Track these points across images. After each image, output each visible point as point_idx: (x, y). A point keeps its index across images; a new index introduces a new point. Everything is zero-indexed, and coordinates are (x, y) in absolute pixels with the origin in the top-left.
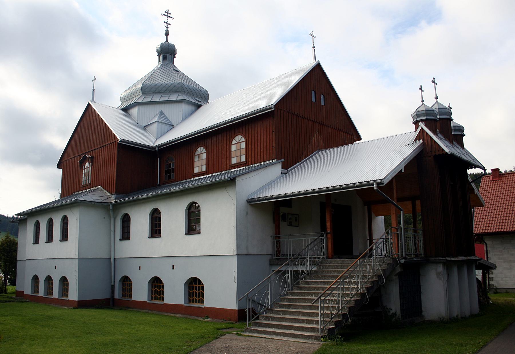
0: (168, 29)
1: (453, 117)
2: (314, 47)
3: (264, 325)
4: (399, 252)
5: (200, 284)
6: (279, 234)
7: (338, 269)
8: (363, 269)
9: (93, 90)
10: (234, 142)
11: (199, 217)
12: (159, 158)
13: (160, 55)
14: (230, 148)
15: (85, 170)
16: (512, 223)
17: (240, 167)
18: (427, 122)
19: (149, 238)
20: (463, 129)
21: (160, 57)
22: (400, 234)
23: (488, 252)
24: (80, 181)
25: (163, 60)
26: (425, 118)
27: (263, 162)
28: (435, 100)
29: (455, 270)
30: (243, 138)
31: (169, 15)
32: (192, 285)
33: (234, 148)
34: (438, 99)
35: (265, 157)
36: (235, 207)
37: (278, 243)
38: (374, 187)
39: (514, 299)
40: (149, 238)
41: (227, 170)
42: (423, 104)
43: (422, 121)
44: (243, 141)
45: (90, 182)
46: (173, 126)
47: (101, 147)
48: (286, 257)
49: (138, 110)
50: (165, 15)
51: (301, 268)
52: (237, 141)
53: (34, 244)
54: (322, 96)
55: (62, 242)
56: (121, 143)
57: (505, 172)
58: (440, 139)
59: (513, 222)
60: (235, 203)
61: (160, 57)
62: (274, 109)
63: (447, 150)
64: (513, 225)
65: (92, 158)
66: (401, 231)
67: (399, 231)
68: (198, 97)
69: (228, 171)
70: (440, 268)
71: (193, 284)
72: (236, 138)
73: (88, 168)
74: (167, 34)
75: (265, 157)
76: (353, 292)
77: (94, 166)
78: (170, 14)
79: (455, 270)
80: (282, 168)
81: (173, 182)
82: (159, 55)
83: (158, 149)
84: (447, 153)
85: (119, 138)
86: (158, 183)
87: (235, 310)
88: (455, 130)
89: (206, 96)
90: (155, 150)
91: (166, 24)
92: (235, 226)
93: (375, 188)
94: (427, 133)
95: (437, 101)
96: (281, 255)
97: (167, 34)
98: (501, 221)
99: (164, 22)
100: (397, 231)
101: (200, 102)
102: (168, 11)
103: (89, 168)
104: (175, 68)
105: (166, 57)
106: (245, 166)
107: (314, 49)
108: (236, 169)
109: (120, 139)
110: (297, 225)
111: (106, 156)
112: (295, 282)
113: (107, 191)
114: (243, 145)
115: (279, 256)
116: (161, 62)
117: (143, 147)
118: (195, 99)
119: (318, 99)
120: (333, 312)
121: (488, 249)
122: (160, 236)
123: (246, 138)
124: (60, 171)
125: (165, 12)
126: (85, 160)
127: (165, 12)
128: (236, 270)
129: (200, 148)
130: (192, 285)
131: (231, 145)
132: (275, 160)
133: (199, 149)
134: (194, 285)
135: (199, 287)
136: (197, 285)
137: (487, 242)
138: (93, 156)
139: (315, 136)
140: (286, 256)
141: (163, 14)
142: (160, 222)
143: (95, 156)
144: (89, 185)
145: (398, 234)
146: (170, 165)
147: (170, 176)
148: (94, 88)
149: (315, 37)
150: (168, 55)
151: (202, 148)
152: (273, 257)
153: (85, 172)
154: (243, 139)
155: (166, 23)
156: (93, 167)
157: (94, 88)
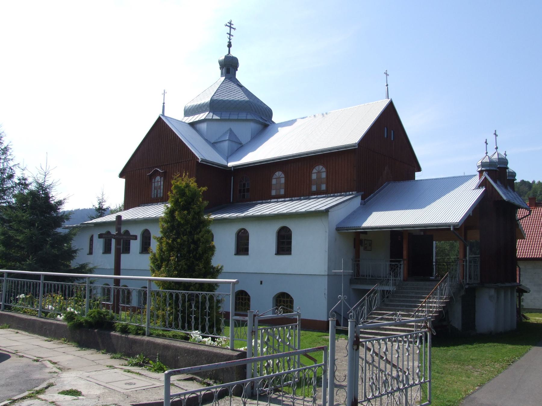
0: (231, 41)
1: (509, 166)
2: (387, 85)
3: (365, 333)
4: (463, 279)
5: (288, 298)
6: (359, 258)
7: (415, 290)
8: (113, 241)
9: (164, 103)
10: (315, 171)
12: (232, 177)
13: (223, 68)
14: (310, 176)
15: (156, 183)
18: (490, 172)
19: (235, 255)
20: (515, 175)
21: (224, 69)
22: (466, 264)
23: (521, 276)
24: (270, 192)
25: (226, 73)
26: (488, 168)
27: (343, 192)
28: (495, 150)
31: (232, 26)
32: (239, 296)
33: (314, 176)
34: (497, 149)
36: (328, 234)
37: (358, 265)
38: (450, 229)
39: (541, 318)
40: (235, 255)
42: (487, 156)
43: (485, 171)
44: (324, 172)
46: (241, 144)
47: (175, 163)
48: (365, 278)
49: (207, 125)
50: (228, 26)
51: (386, 288)
52: (317, 171)
54: (392, 132)
56: (201, 162)
57: (533, 182)
58: (498, 186)
60: (328, 231)
61: (222, 70)
62: (357, 147)
63: (505, 198)
65: (165, 173)
66: (466, 262)
67: (465, 262)
70: (492, 292)
71: (240, 296)
72: (317, 168)
73: (160, 182)
74: (230, 46)
76: (434, 310)
78: (232, 24)
80: (361, 200)
81: (248, 201)
82: (221, 68)
83: (234, 169)
84: (504, 200)
85: (199, 158)
86: (232, 201)
87: (325, 321)
88: (509, 176)
90: (231, 169)
92: (327, 250)
93: (451, 229)
96: (360, 276)
97: (230, 46)
99: (227, 33)
100: (464, 262)
101: (266, 121)
102: (231, 22)
103: (160, 181)
104: (238, 83)
105: (229, 70)
107: (388, 88)
109: (201, 158)
110: (370, 250)
112: (382, 299)
114: (324, 175)
115: (358, 277)
117: (219, 166)
118: (261, 118)
120: (422, 324)
121: (521, 273)
122: (247, 254)
123: (326, 168)
124: (123, 181)
126: (156, 173)
127: (228, 23)
128: (327, 288)
130: (239, 296)
131: (312, 173)
132: (356, 192)
133: (277, 173)
134: (282, 299)
135: (287, 301)
136: (285, 299)
137: (521, 267)
139: (386, 168)
140: (365, 277)
141: (227, 25)
142: (248, 241)
143: (168, 171)
145: (464, 265)
146: (244, 185)
147: (244, 196)
148: (164, 101)
149: (388, 75)
151: (280, 173)
152: (353, 277)
154: (324, 170)
157: (164, 101)
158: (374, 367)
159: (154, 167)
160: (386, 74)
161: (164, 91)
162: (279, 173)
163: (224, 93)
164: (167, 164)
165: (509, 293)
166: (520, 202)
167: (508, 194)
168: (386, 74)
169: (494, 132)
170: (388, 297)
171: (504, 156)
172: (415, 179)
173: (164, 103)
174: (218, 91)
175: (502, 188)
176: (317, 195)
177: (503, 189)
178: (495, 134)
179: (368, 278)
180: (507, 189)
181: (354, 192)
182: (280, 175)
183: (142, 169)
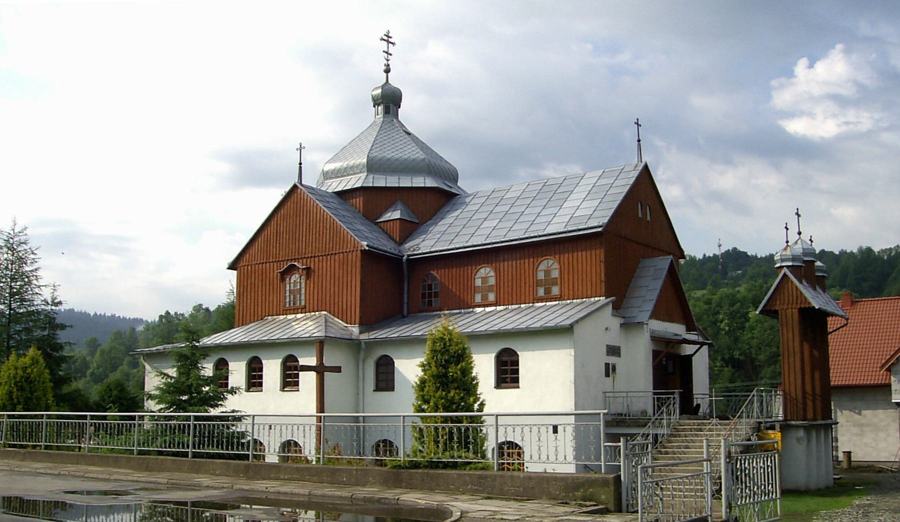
0: (389, 62)
9: (300, 164)
11: (517, 367)
16: (896, 326)
17: (551, 301)
29: (814, 434)
30: (555, 263)
31: (390, 40)
34: (389, 74)
35: (589, 292)
41: (529, 303)
43: (787, 267)
45: (303, 303)
48: (624, 417)
50: (384, 40)
53: (374, 391)
55: (375, 392)
59: (898, 324)
64: (898, 328)
65: (308, 269)
68: (446, 178)
69: (531, 305)
74: (387, 71)
75: (589, 292)
77: (312, 281)
78: (390, 37)
79: (814, 434)
89: (456, 178)
91: (386, 55)
94: (796, 287)
95: (800, 238)
97: (387, 71)
98: (862, 362)
99: (384, 51)
101: (451, 187)
106: (559, 301)
108: (544, 304)
111: (337, 269)
113: (342, 321)
116: (382, 116)
119: (644, 214)
125: (385, 35)
127: (385, 35)
129: (484, 269)
132: (604, 298)
138: (309, 266)
143: (312, 267)
144: (302, 309)
147: (430, 303)
148: (300, 161)
150: (391, 105)
153: (292, 288)
155: (386, 52)
156: (308, 282)
157: (300, 161)
158: (805, 343)
159: (291, 260)
160: (638, 124)
161: (301, 146)
162: (490, 271)
163: (385, 146)
164: (311, 257)
165: (823, 434)
166: (834, 308)
167: (817, 297)
168: (638, 124)
169: (796, 211)
170: (661, 442)
171: (810, 242)
172: (482, 295)
173: (300, 164)
174: (376, 142)
175: (809, 289)
176: (546, 302)
177: (812, 291)
178: (797, 214)
179: (627, 418)
180: (816, 290)
181: (601, 298)
182: (488, 273)
183: (266, 263)
